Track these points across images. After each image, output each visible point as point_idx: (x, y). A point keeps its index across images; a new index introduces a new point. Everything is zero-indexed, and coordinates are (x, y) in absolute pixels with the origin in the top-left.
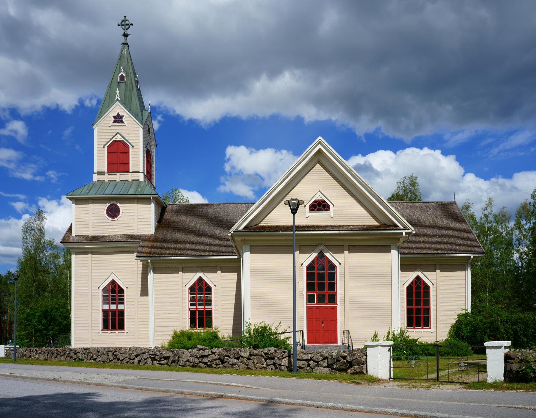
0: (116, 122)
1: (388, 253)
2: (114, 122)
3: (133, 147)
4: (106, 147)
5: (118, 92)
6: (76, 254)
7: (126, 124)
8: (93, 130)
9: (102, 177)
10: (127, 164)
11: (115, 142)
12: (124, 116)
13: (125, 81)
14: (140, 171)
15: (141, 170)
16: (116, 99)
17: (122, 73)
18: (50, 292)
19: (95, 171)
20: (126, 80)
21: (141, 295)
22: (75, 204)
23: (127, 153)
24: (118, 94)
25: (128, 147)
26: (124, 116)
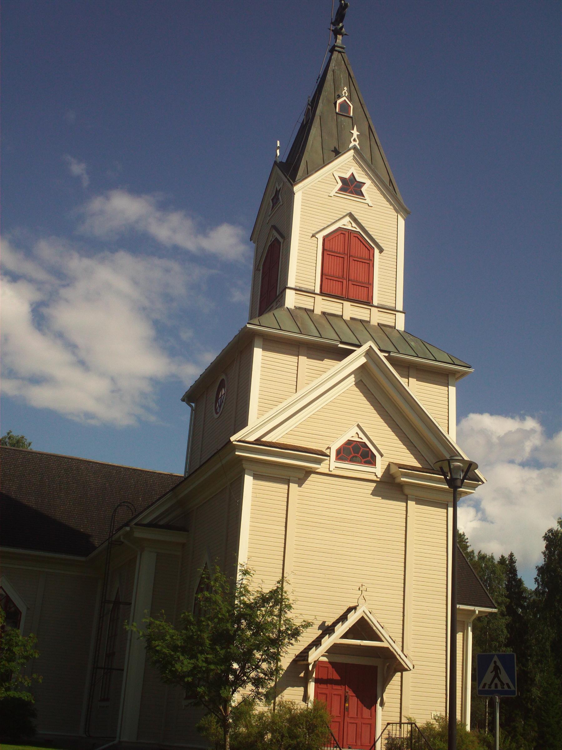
0: (346, 192)
1: (283, 443)
2: (341, 189)
3: (381, 250)
4: (320, 236)
5: (355, 132)
6: (257, 477)
7: (368, 201)
8: (292, 194)
9: (306, 302)
10: (368, 285)
11: (340, 230)
12: (364, 183)
13: (351, 114)
14: (294, 292)
15: (400, 307)
16: (351, 145)
17: (344, 98)
18: (220, 578)
19: (291, 282)
20: (353, 115)
21: (363, 616)
22: (261, 350)
23: (369, 263)
24: (355, 136)
25: (370, 250)
26: (364, 183)
